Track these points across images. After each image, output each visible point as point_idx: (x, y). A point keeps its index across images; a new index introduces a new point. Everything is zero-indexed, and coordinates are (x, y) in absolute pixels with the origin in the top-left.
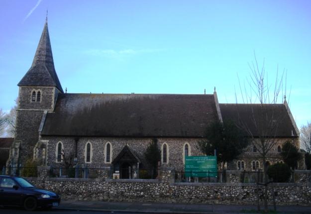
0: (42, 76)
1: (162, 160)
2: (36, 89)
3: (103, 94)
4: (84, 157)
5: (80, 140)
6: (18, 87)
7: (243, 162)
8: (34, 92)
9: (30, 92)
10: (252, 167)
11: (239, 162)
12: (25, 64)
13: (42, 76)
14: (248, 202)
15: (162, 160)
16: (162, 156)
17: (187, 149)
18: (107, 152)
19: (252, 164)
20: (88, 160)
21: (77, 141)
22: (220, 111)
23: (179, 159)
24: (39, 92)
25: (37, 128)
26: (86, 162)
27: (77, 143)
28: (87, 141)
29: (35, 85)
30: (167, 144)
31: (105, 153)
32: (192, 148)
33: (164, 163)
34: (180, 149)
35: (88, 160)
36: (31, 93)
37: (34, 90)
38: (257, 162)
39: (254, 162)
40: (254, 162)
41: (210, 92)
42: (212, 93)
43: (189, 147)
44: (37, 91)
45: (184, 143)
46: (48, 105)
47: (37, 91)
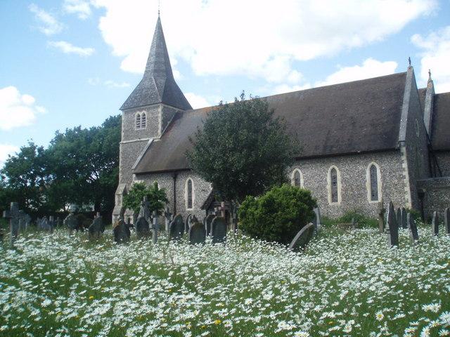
3: (277, 96)
4: (185, 201)
5: (179, 176)
8: (139, 116)
9: (134, 115)
17: (373, 176)
20: (190, 206)
21: (175, 179)
22: (408, 100)
23: (321, 197)
24: (144, 115)
25: (395, 132)
26: (331, 204)
27: (175, 181)
28: (187, 177)
29: (138, 108)
32: (342, 176)
33: (333, 204)
34: (323, 180)
35: (190, 206)
36: (135, 118)
37: (138, 112)
41: (53, 136)
42: (404, 70)
43: (338, 174)
44: (141, 114)
46: (153, 133)
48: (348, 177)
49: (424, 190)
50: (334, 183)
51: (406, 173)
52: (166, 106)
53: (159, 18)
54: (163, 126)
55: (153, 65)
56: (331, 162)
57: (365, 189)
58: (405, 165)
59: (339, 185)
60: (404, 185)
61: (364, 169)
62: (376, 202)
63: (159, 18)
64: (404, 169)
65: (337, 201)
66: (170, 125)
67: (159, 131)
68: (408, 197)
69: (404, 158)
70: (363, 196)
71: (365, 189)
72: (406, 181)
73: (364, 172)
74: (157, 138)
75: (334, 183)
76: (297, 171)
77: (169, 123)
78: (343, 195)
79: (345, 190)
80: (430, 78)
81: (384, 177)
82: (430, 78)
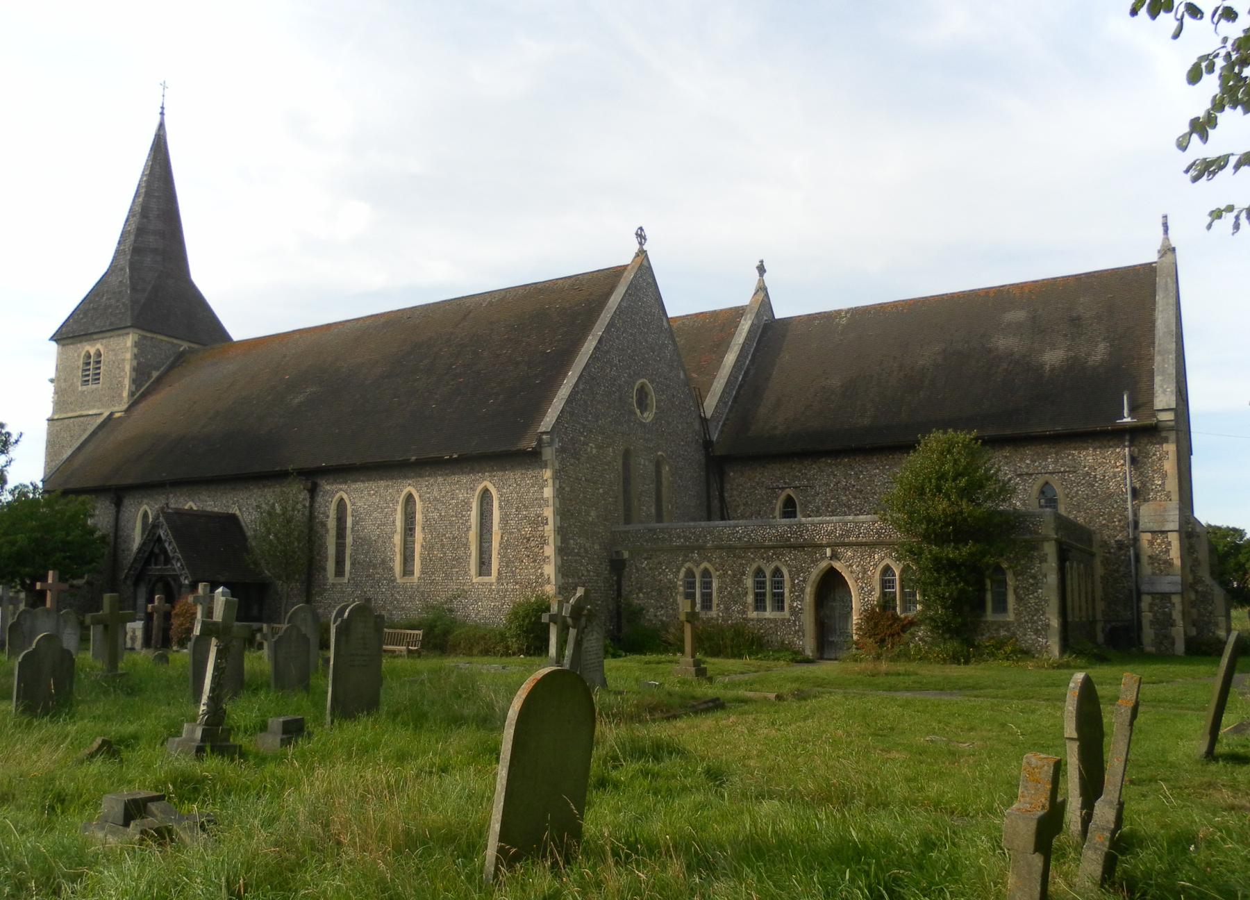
0: (149, 286)
1: (331, 565)
2: (93, 346)
5: (126, 502)
6: (54, 344)
7: (706, 574)
10: (750, 599)
11: (690, 573)
12: (88, 253)
13: (149, 286)
14: (323, 781)
15: (331, 565)
16: (331, 550)
18: (412, 535)
19: (749, 582)
21: (118, 504)
27: (118, 512)
28: (140, 504)
30: (345, 496)
31: (473, 535)
38: (777, 572)
39: (759, 572)
40: (759, 572)
42: (1149, 255)
44: (92, 352)
45: (399, 492)
47: (92, 352)
48: (436, 515)
49: (626, 555)
50: (409, 529)
51: (549, 512)
52: (149, 335)
53: (161, 126)
54: (136, 382)
55: (132, 237)
56: (406, 477)
57: (466, 546)
58: (548, 492)
59: (419, 535)
60: (544, 542)
61: (465, 491)
62: (486, 579)
63: (161, 126)
64: (547, 500)
65: (490, 574)
66: (159, 380)
67: (125, 394)
68: (550, 570)
69: (548, 474)
70: (461, 561)
71: (466, 546)
72: (549, 530)
73: (467, 504)
74: (119, 409)
75: (409, 529)
76: (342, 499)
77: (155, 374)
78: (423, 560)
79: (428, 547)
80: (761, 281)
81: (504, 520)
82: (761, 281)
